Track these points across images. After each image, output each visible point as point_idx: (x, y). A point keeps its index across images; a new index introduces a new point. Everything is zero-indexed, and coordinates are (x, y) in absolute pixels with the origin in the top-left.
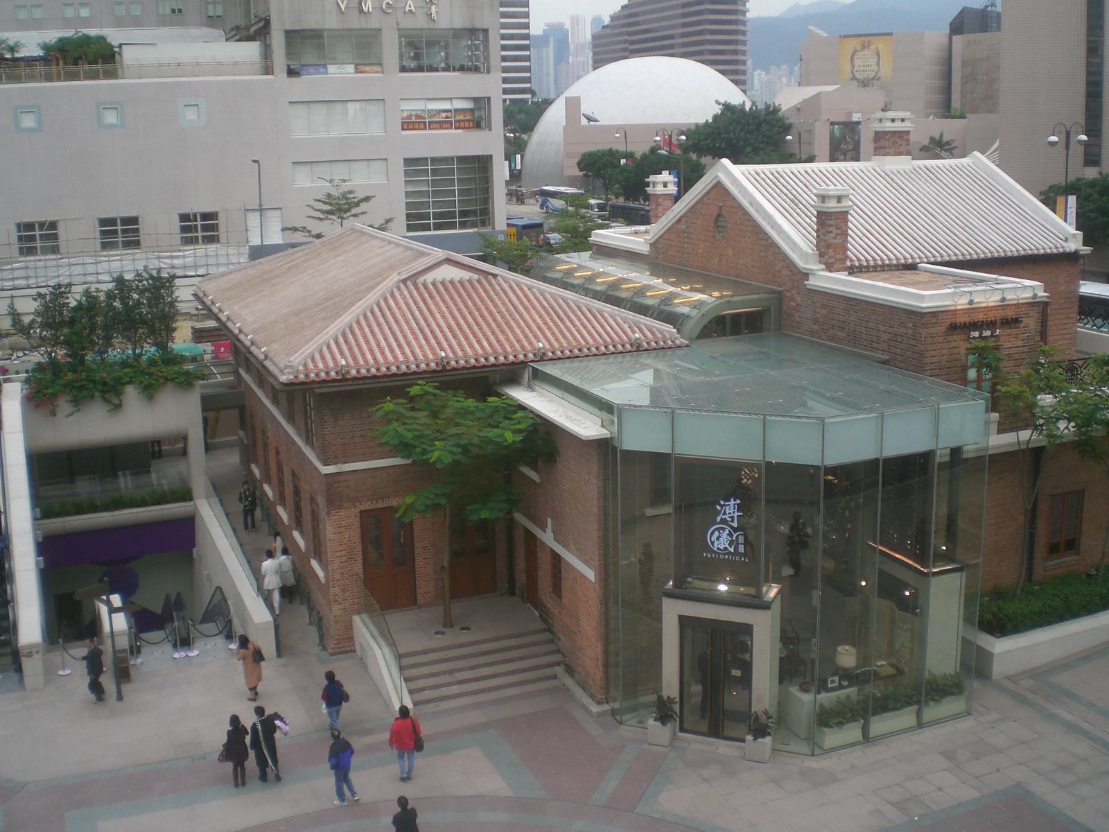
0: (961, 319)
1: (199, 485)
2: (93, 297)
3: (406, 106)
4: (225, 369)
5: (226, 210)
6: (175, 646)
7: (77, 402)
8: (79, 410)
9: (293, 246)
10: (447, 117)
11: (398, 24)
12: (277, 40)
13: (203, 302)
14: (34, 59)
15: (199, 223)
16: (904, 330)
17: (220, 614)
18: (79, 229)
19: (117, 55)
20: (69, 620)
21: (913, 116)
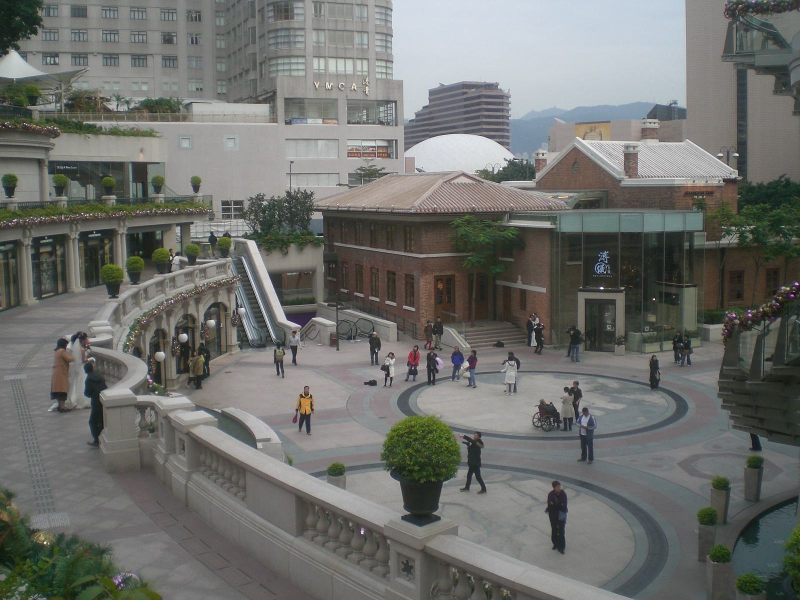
0: (690, 190)
3: (351, 143)
10: (373, 150)
11: (347, 97)
12: (280, 103)
16: (666, 196)
21: (659, 121)
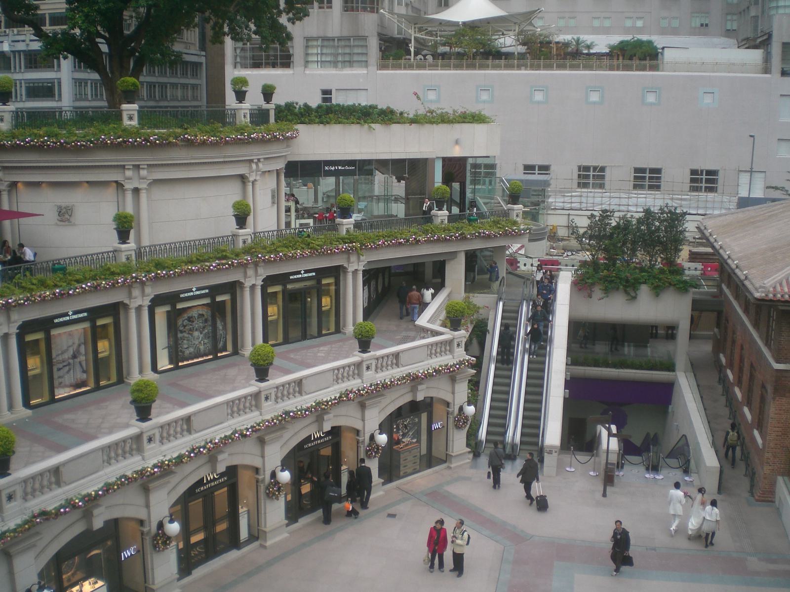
1: (681, 361)
2: (628, 221)
4: (710, 283)
5: (725, 170)
6: (647, 469)
7: (607, 291)
8: (607, 297)
9: (774, 200)
12: (776, 49)
13: (703, 233)
14: (603, 55)
15: (704, 177)
17: (682, 456)
18: (619, 173)
19: (660, 54)
20: (578, 437)
